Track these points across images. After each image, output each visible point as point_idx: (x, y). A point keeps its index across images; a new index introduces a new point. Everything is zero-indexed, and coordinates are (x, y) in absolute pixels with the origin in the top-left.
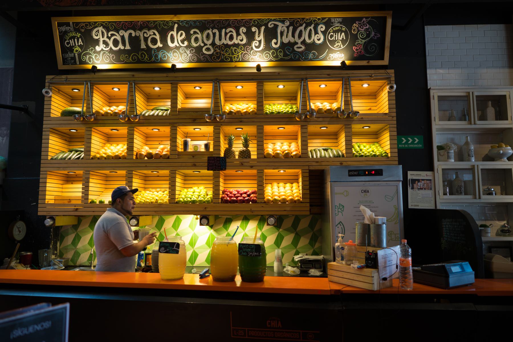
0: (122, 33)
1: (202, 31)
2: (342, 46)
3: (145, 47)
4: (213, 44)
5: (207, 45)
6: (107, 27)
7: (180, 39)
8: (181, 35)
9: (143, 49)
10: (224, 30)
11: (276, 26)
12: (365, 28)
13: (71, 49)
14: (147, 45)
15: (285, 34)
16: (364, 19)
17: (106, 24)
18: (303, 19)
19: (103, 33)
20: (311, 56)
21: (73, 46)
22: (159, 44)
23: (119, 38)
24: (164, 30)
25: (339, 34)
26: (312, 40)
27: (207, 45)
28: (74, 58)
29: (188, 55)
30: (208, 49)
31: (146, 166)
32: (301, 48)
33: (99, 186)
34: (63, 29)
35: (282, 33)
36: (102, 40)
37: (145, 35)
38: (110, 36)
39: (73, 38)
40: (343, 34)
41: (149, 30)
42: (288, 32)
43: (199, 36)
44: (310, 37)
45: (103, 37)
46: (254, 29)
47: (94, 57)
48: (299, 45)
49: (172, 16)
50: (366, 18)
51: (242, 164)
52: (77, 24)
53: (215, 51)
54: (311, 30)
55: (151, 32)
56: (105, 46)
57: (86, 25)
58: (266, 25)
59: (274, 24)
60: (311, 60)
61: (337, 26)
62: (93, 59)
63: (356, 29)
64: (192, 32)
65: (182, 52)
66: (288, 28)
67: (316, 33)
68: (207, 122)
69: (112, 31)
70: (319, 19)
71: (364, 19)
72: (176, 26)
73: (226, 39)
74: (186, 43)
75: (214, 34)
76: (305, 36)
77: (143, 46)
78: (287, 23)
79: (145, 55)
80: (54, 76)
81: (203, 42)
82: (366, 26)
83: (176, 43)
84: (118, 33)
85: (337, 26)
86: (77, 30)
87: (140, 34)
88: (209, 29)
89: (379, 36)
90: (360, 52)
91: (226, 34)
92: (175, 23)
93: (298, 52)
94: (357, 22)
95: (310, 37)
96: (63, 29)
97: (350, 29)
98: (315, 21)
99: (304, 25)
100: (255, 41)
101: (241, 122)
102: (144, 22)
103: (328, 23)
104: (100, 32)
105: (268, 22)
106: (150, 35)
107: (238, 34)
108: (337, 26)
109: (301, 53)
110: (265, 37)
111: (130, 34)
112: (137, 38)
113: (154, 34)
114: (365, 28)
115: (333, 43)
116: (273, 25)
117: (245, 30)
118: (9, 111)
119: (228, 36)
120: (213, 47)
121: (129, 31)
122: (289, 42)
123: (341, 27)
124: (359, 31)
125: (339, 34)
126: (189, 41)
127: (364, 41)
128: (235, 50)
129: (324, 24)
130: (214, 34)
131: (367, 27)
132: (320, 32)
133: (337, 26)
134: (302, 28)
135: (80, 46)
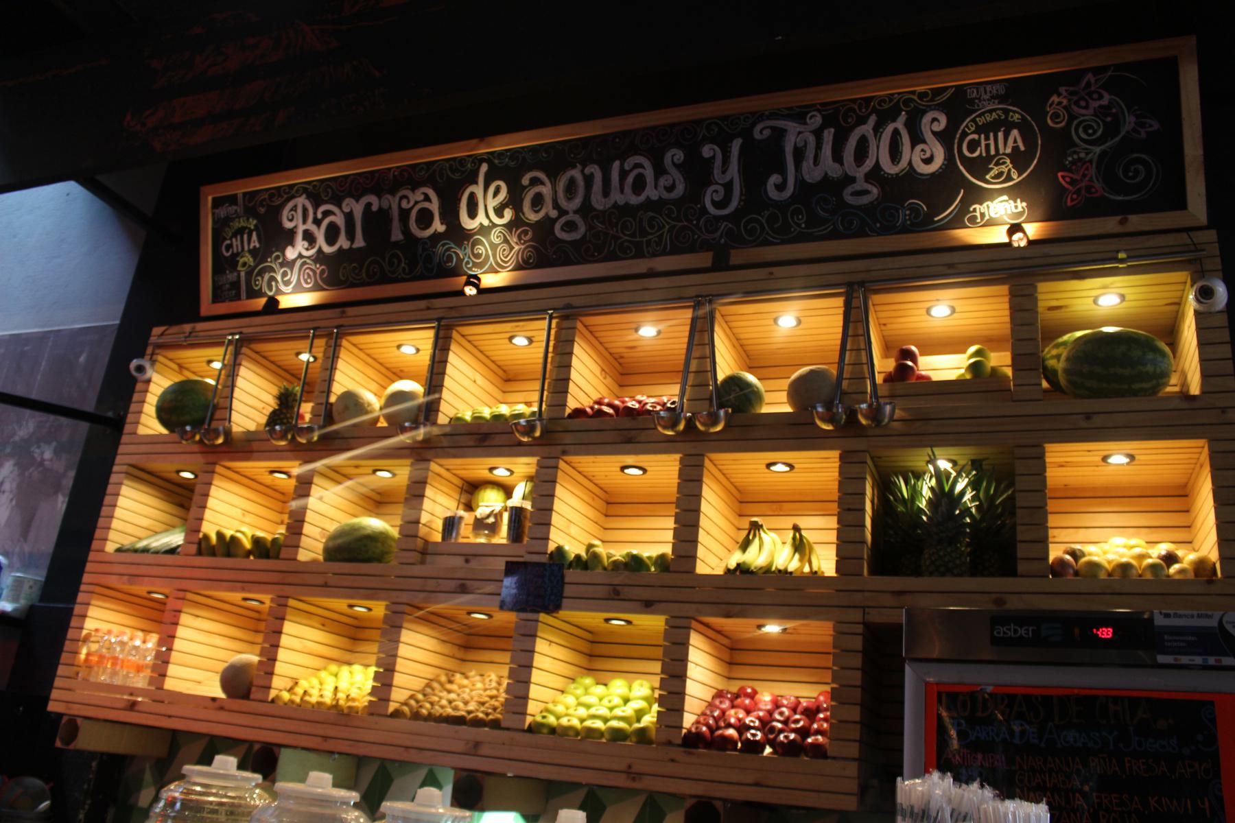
0: (349, 204)
1: (553, 176)
2: (1014, 175)
3: (401, 237)
4: (586, 209)
5: (566, 213)
6: (316, 194)
7: (492, 203)
8: (496, 194)
9: (396, 244)
10: (617, 164)
11: (779, 134)
12: (1096, 104)
13: (233, 262)
14: (406, 231)
15: (810, 153)
16: (1090, 77)
17: (315, 186)
18: (868, 100)
19: (305, 210)
20: (903, 215)
21: (238, 254)
22: (438, 226)
23: (339, 219)
24: (452, 187)
25: (1000, 135)
26: (904, 163)
27: (566, 213)
28: (236, 285)
29: (512, 248)
30: (570, 226)
31: (326, 585)
32: (866, 192)
33: (219, 641)
34: (222, 212)
35: (799, 154)
36: (301, 228)
37: (405, 205)
38: (319, 216)
39: (240, 231)
40: (1015, 132)
41: (413, 190)
42: (819, 147)
43: (546, 190)
44: (895, 154)
45: (304, 222)
46: (706, 151)
47: (279, 278)
48: (861, 185)
49: (474, 141)
50: (1097, 71)
51: (617, 593)
52: (251, 195)
53: (590, 228)
54: (896, 132)
55: (418, 196)
56: (306, 244)
57: (271, 196)
58: (747, 134)
59: (773, 129)
60: (905, 230)
61: (990, 110)
62: (277, 282)
63: (1062, 112)
64: (525, 181)
65: (497, 241)
66: (818, 134)
67: (917, 139)
68: (520, 444)
69: (326, 202)
70: (922, 95)
71: (1090, 77)
72: (484, 168)
73: (622, 191)
74: (508, 214)
75: (589, 180)
76: (880, 153)
77: (397, 235)
78: (816, 120)
79: (400, 261)
80: (163, 328)
81: (556, 206)
82: (1101, 97)
83: (481, 219)
84: (340, 207)
85: (991, 111)
86: (250, 212)
87: (392, 203)
88: (574, 167)
89: (1156, 126)
90: (1089, 189)
91: (623, 174)
92: (482, 161)
93: (859, 207)
94: (1062, 90)
95: (895, 154)
96: (222, 212)
97: (1040, 117)
98: (907, 102)
99: (873, 120)
100: (713, 188)
101: (629, 441)
102: (402, 169)
103: (958, 106)
104: (300, 210)
105: (753, 125)
106: (416, 203)
107: (660, 171)
108: (991, 111)
109: (870, 209)
110: (744, 169)
111: (369, 205)
112: (384, 214)
113: (427, 198)
114: (1096, 104)
115: (980, 167)
116: (767, 133)
117: (679, 156)
118: (84, 426)
119: (630, 179)
120: (584, 217)
121: (365, 199)
122: (826, 177)
123: (1006, 112)
124: (1072, 117)
125: (1000, 135)
126: (518, 209)
127: (1098, 150)
128: (651, 219)
129: (942, 107)
130: (589, 180)
131: (1105, 101)
132: (928, 136)
133: (990, 110)
134: (867, 129)
135: (254, 252)
